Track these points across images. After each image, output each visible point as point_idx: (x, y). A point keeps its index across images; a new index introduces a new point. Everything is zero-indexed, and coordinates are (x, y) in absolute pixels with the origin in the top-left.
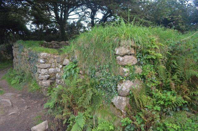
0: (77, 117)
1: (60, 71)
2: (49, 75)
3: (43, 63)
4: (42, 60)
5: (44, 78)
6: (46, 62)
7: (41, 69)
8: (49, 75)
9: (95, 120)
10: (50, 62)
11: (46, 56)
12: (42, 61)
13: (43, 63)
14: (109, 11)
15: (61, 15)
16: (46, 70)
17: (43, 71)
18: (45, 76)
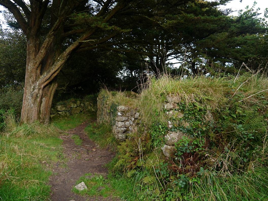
0: (5, 123)
1: (133, 124)
2: (125, 129)
3: (120, 116)
4: (119, 113)
5: (121, 131)
6: (123, 115)
7: (119, 122)
8: (125, 129)
9: (164, 186)
10: (127, 116)
11: (123, 109)
12: (119, 114)
13: (120, 116)
14: (141, 55)
15: (157, 60)
16: (123, 123)
17: (120, 124)
18: (122, 129)
